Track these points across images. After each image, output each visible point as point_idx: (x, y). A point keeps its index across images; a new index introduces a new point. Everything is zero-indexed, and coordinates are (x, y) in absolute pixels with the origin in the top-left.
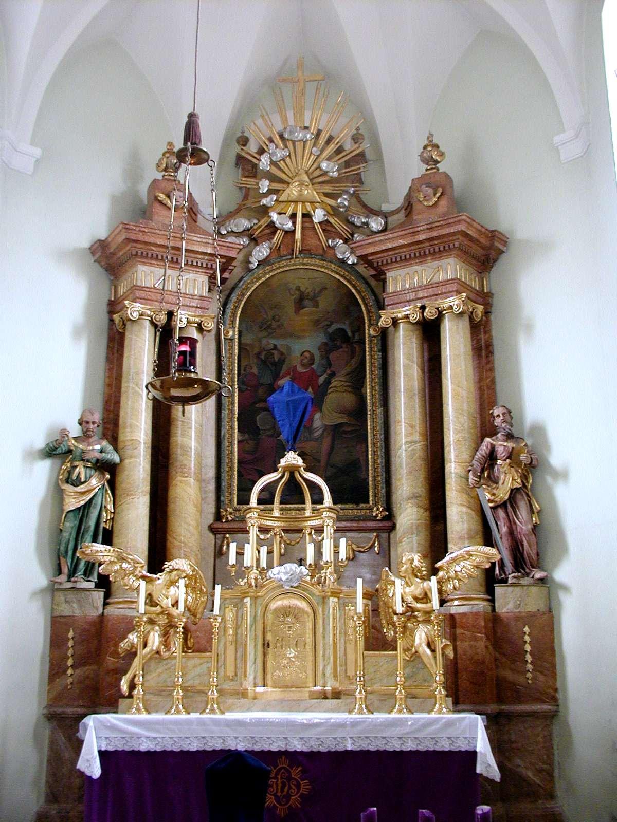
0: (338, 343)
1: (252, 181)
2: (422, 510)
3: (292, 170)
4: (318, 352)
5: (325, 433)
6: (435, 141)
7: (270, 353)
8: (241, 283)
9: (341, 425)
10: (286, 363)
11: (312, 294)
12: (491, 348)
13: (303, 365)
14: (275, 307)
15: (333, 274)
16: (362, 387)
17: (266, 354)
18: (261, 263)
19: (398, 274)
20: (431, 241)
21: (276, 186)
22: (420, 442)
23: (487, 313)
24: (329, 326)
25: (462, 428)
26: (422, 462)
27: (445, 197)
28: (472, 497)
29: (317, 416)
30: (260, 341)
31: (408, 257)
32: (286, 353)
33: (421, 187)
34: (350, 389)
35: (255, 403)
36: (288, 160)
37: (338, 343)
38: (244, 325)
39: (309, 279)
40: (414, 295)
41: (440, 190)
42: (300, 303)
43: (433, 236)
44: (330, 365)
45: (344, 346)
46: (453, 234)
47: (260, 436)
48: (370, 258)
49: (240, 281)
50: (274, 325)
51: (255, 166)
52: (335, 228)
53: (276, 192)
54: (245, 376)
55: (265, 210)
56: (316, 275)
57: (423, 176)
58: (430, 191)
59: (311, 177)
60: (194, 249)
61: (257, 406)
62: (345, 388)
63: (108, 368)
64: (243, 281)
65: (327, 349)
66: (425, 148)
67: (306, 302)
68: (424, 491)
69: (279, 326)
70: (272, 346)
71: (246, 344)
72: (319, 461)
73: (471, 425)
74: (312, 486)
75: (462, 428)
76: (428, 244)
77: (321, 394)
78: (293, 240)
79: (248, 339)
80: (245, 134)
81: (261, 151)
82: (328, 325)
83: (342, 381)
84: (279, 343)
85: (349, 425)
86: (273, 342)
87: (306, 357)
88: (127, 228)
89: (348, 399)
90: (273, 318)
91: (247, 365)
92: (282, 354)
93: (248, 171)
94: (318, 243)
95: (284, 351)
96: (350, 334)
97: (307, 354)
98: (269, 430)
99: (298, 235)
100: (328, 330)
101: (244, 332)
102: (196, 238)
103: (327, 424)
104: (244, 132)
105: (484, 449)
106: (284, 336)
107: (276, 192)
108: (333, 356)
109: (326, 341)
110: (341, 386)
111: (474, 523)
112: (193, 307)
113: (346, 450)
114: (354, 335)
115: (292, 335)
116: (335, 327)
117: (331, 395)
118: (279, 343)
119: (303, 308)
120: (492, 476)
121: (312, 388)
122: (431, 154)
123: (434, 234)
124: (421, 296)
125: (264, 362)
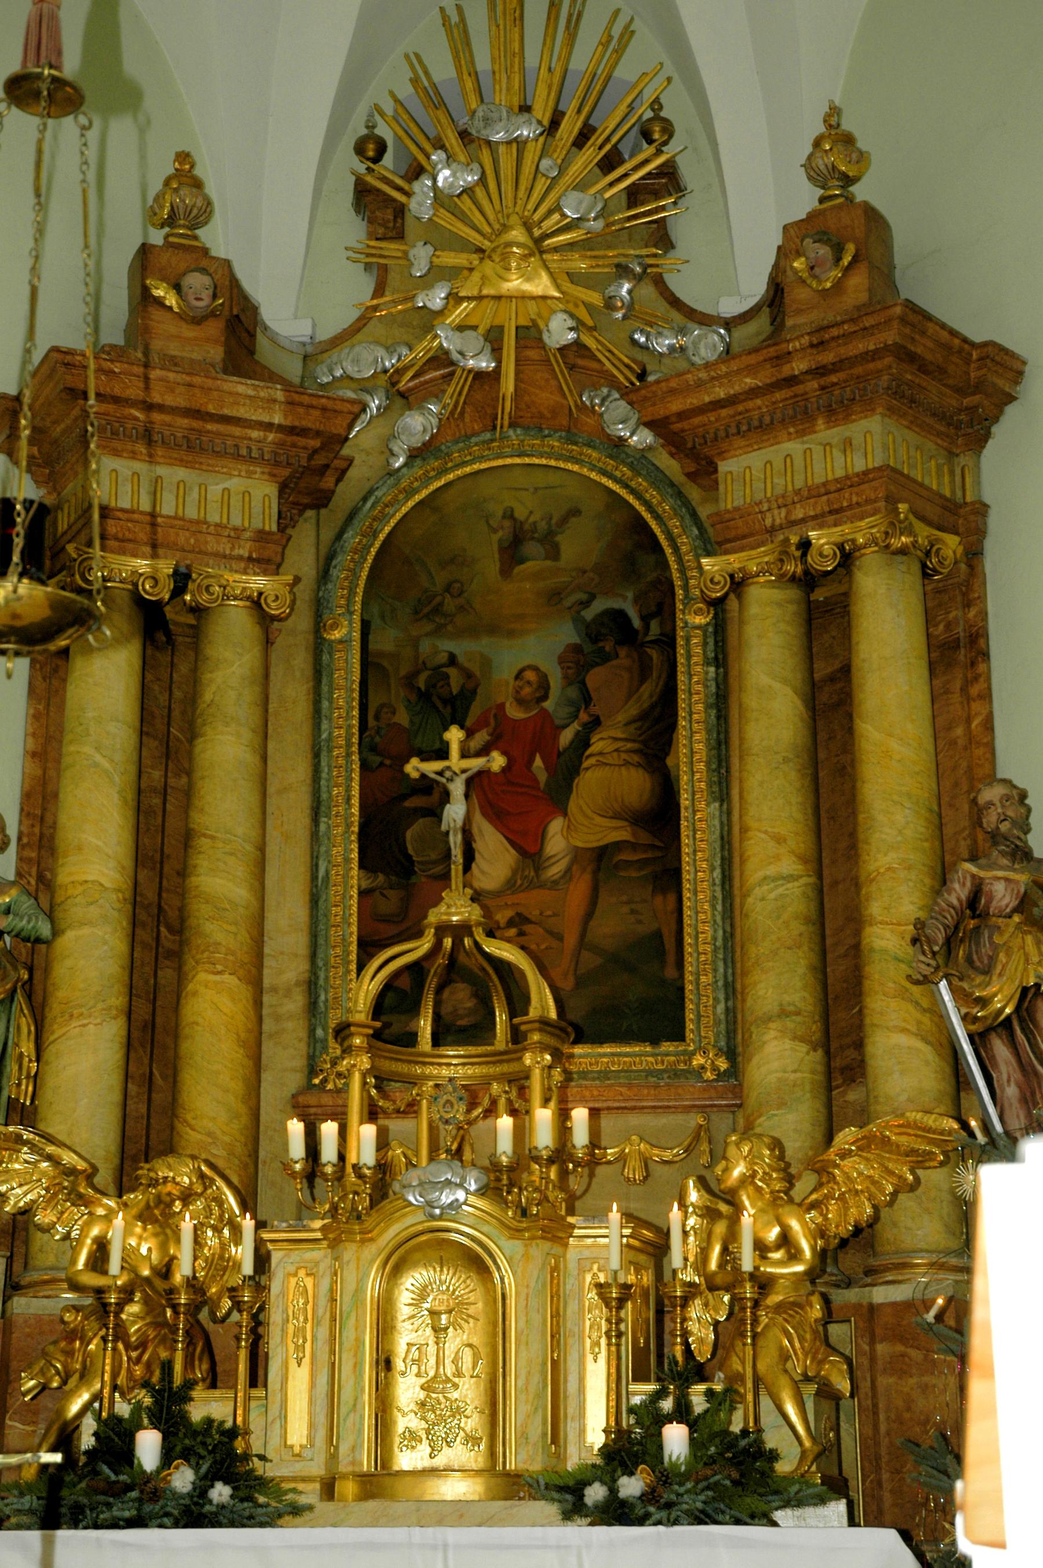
0: (608, 646)
1: (392, 248)
2: (804, 1048)
3: (491, 217)
4: (558, 670)
5: (575, 868)
6: (847, 125)
7: (439, 675)
8: (369, 504)
9: (618, 846)
10: (478, 698)
11: (543, 526)
12: (982, 641)
13: (521, 702)
14: (452, 560)
15: (593, 475)
16: (667, 754)
17: (430, 677)
18: (415, 455)
19: (745, 464)
20: (823, 375)
21: (449, 259)
22: (801, 877)
23: (974, 554)
24: (586, 604)
25: (899, 838)
26: (803, 928)
27: (862, 268)
28: (925, 1010)
29: (556, 826)
30: (415, 643)
31: (767, 419)
32: (478, 674)
33: (802, 241)
34: (636, 758)
35: (405, 797)
36: (480, 193)
37: (608, 646)
38: (375, 609)
39: (536, 489)
40: (783, 515)
41: (851, 249)
42: (512, 552)
43: (825, 361)
44: (587, 699)
45: (623, 652)
46: (873, 355)
47: (414, 879)
48: (677, 427)
49: (365, 499)
50: (450, 604)
51: (400, 211)
52: (599, 361)
53: (452, 274)
54: (378, 732)
55: (427, 321)
56: (553, 479)
57: (812, 216)
58: (824, 251)
59: (537, 232)
60: (239, 415)
61: (407, 804)
62: (624, 756)
63: (32, 711)
64: (372, 499)
65: (579, 662)
66: (817, 143)
67: (531, 548)
68: (811, 1000)
69: (461, 608)
70: (443, 658)
71: (381, 654)
72: (560, 938)
73: (923, 830)
74: (502, 967)
75: (899, 838)
76: (815, 384)
77: (567, 769)
78: (495, 399)
79: (385, 641)
80: (377, 131)
81: (417, 172)
82: (581, 603)
83: (616, 739)
84: (461, 648)
85: (633, 846)
86: (448, 645)
87: (529, 683)
88: (68, 364)
89: (634, 785)
90: (448, 589)
91: (382, 706)
92: (469, 675)
93: (384, 225)
94: (559, 399)
95: (475, 668)
96: (637, 623)
97: (530, 675)
98: (435, 863)
99: (508, 385)
100: (583, 613)
101: (376, 623)
102: (243, 387)
103: (580, 844)
104: (374, 127)
105: (959, 892)
106: (472, 632)
107: (452, 274)
108: (594, 678)
109: (578, 641)
110: (616, 750)
111: (933, 1076)
112: (240, 558)
113: (625, 909)
114: (647, 628)
115: (493, 630)
116: (599, 605)
117: (589, 773)
118: (461, 648)
119: (522, 561)
120: (975, 957)
121: (543, 758)
122: (836, 157)
123: (828, 357)
124: (801, 516)
125: (425, 696)
